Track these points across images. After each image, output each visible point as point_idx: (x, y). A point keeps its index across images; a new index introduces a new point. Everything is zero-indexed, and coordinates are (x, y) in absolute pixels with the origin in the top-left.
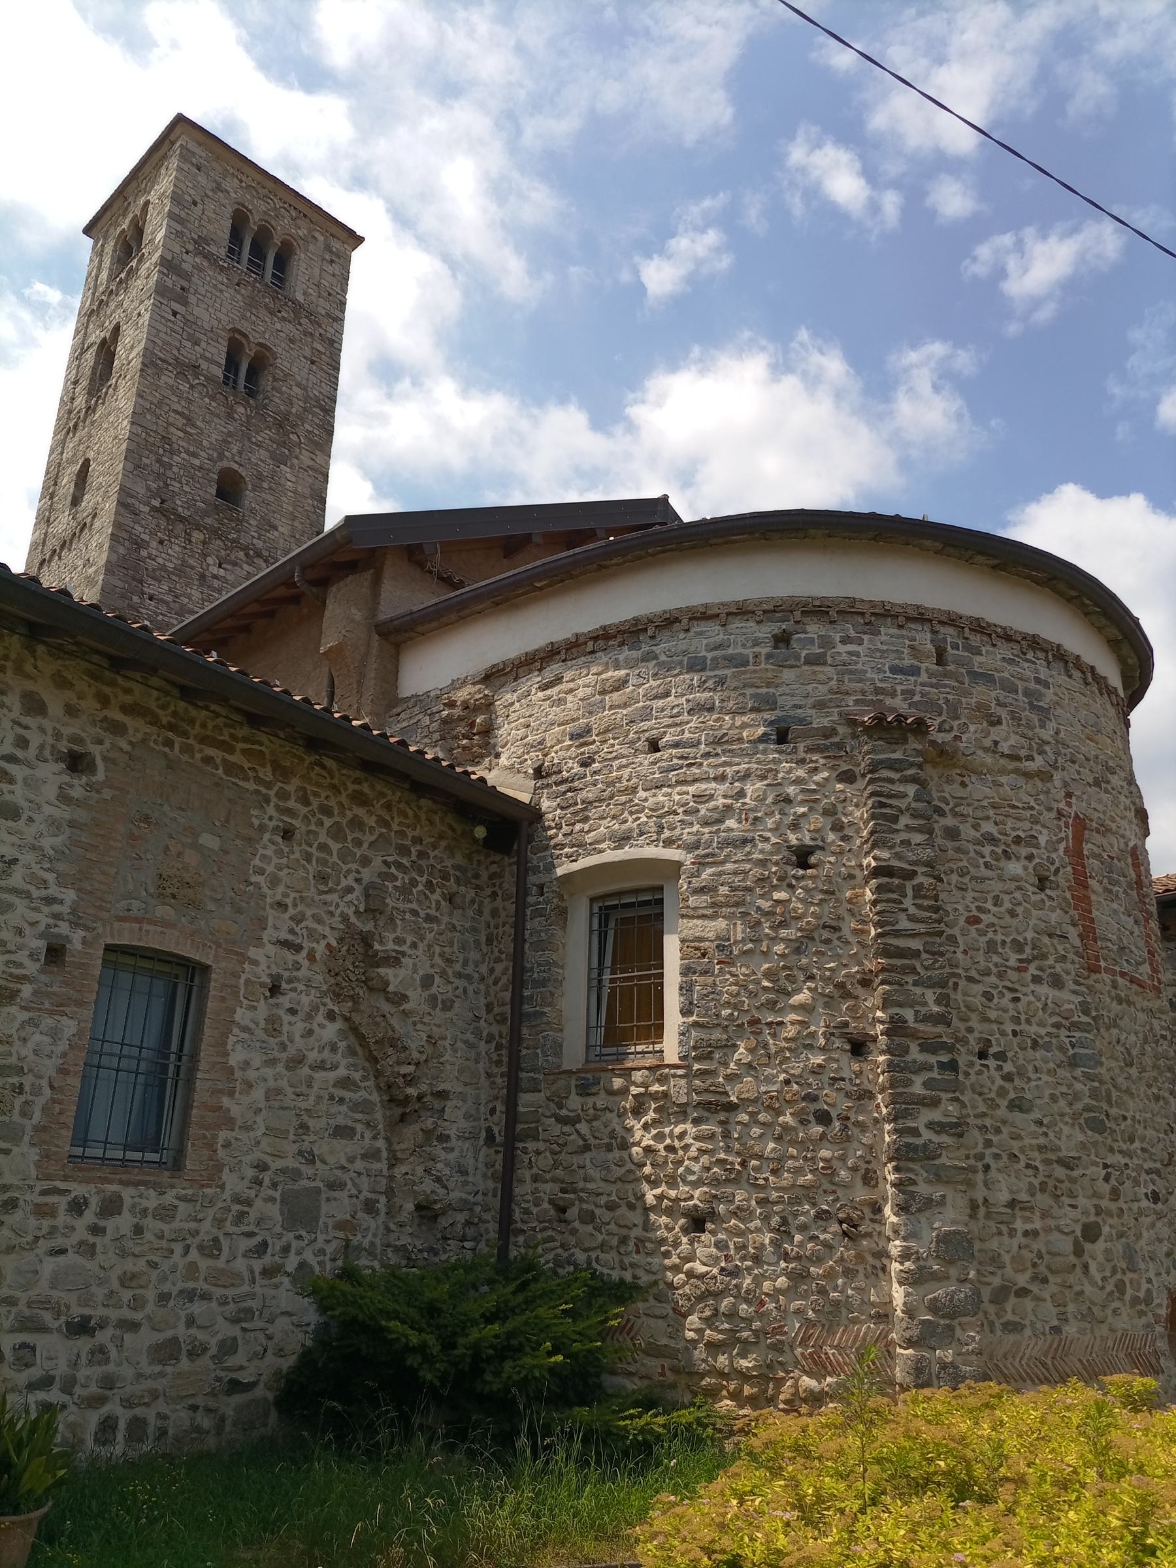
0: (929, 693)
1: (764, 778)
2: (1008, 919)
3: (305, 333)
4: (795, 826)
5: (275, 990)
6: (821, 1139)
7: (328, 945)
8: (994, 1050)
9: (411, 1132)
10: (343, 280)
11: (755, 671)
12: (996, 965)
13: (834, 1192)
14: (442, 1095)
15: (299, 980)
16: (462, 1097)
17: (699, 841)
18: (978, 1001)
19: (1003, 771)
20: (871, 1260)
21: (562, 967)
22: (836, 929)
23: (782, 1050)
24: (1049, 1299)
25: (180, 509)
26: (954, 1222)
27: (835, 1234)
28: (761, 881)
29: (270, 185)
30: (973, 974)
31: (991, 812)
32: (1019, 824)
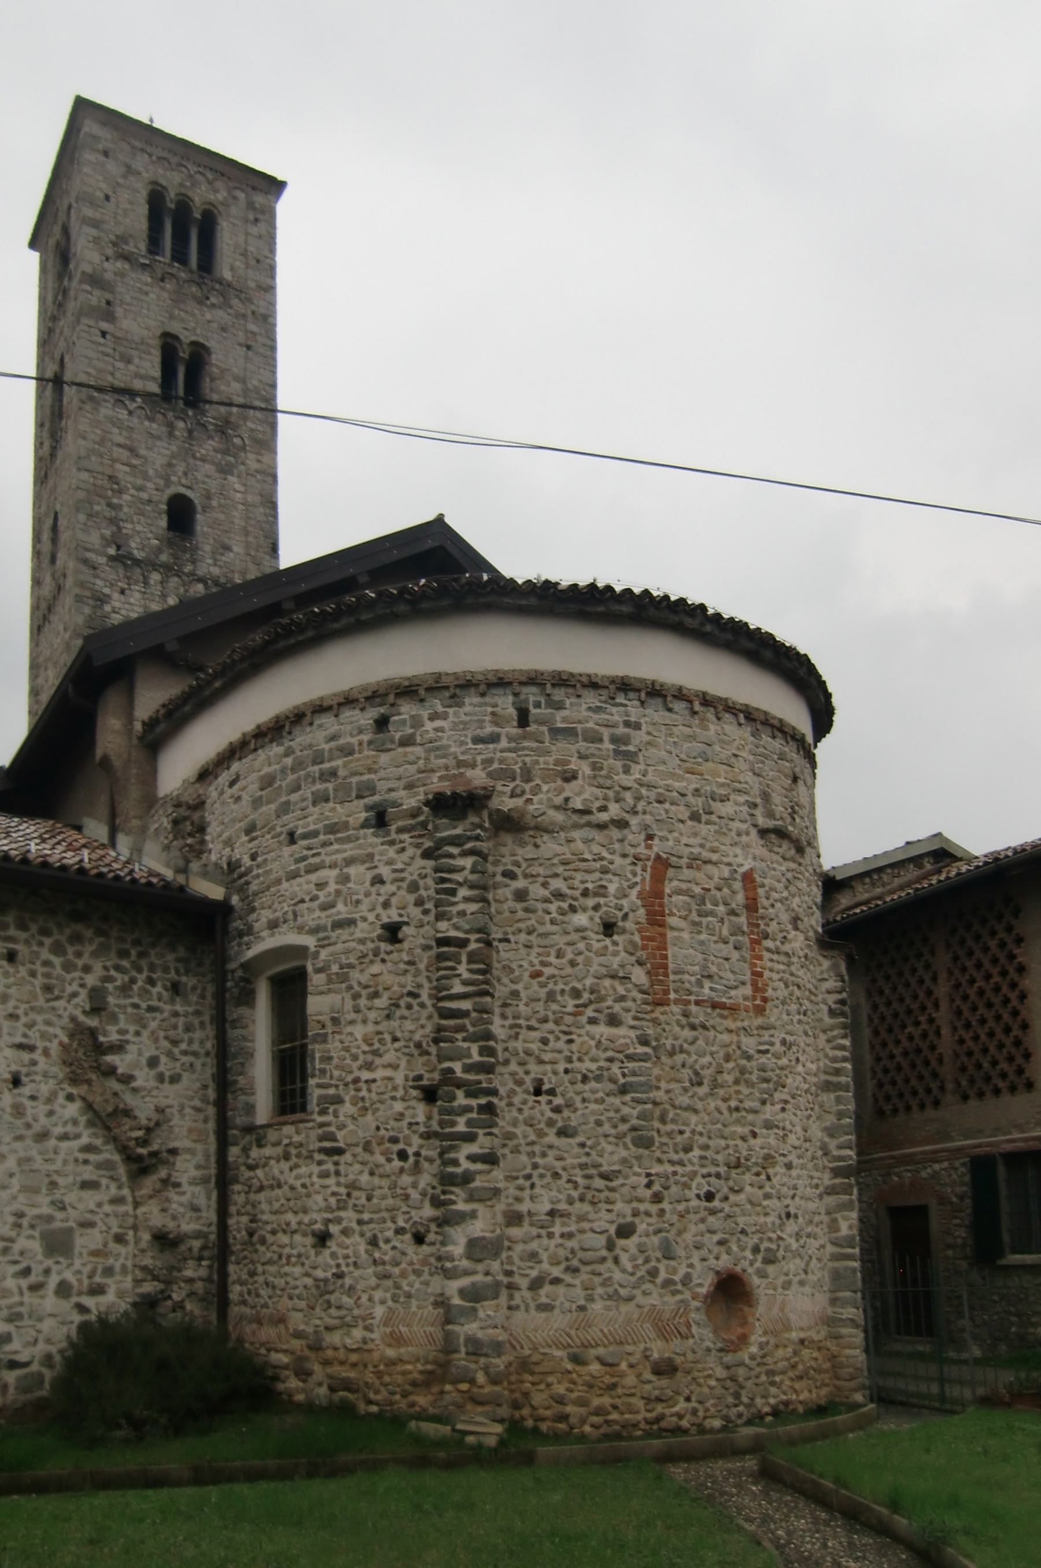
2: (569, 970)
5: (16, 1082)
7: (61, 1044)
8: (545, 1087)
9: (150, 1183)
11: (358, 760)
12: (554, 1013)
14: (173, 1152)
15: (36, 1073)
16: (191, 1151)
18: (535, 1047)
19: (576, 826)
25: (135, 552)
26: (483, 1231)
30: (533, 1023)
31: (560, 869)
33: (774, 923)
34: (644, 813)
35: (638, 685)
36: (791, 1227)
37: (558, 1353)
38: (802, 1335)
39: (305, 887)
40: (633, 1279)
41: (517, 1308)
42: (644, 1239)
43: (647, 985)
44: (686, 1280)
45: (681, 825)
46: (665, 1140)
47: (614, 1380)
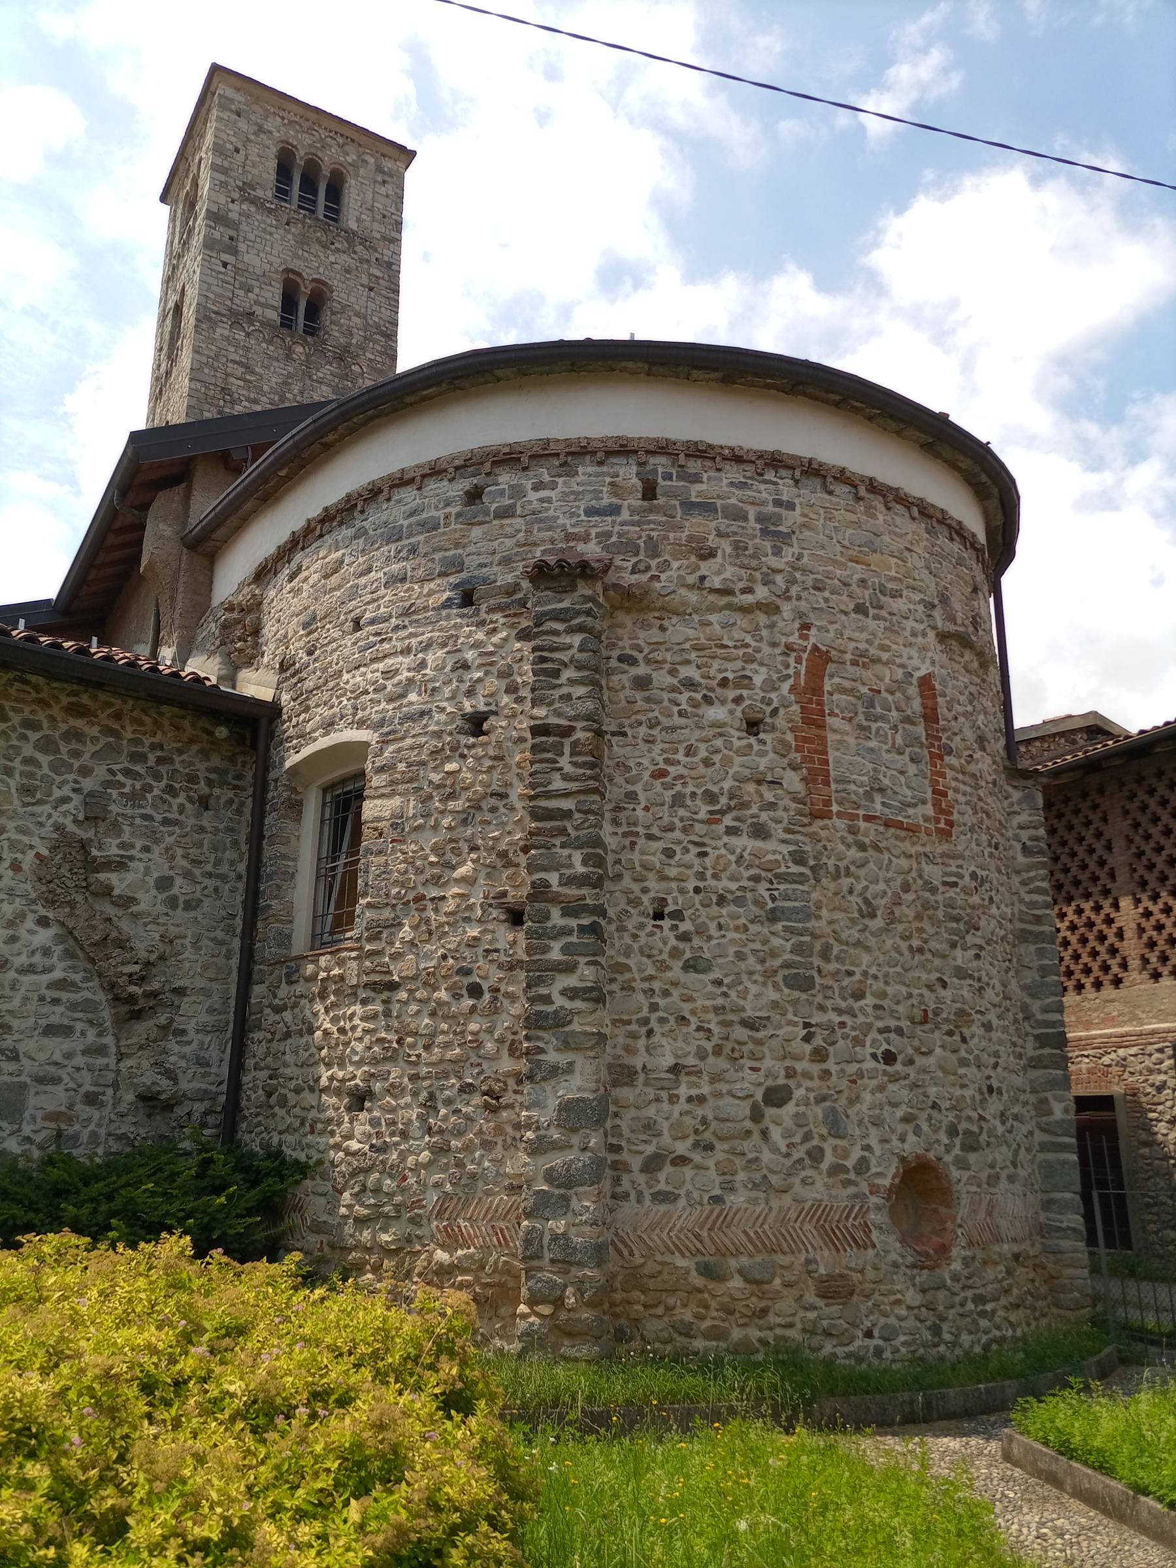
0: (628, 532)
1: (444, 645)
2: (702, 769)
3: (361, 261)
4: (470, 693)
6: (471, 1013)
7: (38, 855)
9: (142, 1029)
10: (398, 199)
11: (444, 533)
12: (682, 820)
13: (480, 1065)
14: (180, 992)
17: (383, 719)
18: (656, 860)
19: (712, 609)
20: (509, 1129)
21: (295, 860)
22: (502, 796)
23: (441, 925)
24: (713, 1167)
26: (579, 1090)
27: (477, 1107)
28: (435, 753)
29: (313, 116)
30: (655, 830)
31: (693, 656)
32: (729, 666)
33: (957, 739)
34: (799, 598)
35: (790, 462)
36: (994, 1105)
37: (681, 1262)
38: (1016, 1248)
39: (369, 676)
40: (788, 1162)
41: (626, 1196)
42: (802, 1109)
43: (803, 793)
44: (862, 1166)
45: (844, 617)
46: (829, 982)
47: (763, 1304)
